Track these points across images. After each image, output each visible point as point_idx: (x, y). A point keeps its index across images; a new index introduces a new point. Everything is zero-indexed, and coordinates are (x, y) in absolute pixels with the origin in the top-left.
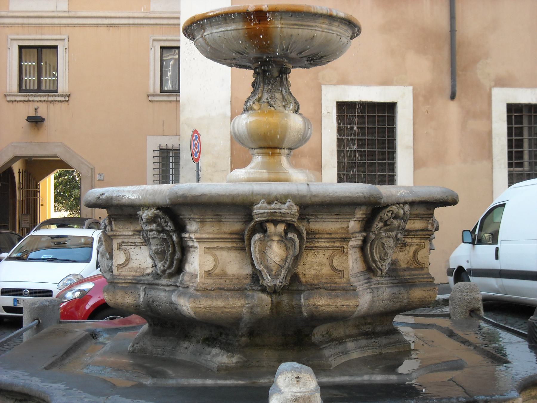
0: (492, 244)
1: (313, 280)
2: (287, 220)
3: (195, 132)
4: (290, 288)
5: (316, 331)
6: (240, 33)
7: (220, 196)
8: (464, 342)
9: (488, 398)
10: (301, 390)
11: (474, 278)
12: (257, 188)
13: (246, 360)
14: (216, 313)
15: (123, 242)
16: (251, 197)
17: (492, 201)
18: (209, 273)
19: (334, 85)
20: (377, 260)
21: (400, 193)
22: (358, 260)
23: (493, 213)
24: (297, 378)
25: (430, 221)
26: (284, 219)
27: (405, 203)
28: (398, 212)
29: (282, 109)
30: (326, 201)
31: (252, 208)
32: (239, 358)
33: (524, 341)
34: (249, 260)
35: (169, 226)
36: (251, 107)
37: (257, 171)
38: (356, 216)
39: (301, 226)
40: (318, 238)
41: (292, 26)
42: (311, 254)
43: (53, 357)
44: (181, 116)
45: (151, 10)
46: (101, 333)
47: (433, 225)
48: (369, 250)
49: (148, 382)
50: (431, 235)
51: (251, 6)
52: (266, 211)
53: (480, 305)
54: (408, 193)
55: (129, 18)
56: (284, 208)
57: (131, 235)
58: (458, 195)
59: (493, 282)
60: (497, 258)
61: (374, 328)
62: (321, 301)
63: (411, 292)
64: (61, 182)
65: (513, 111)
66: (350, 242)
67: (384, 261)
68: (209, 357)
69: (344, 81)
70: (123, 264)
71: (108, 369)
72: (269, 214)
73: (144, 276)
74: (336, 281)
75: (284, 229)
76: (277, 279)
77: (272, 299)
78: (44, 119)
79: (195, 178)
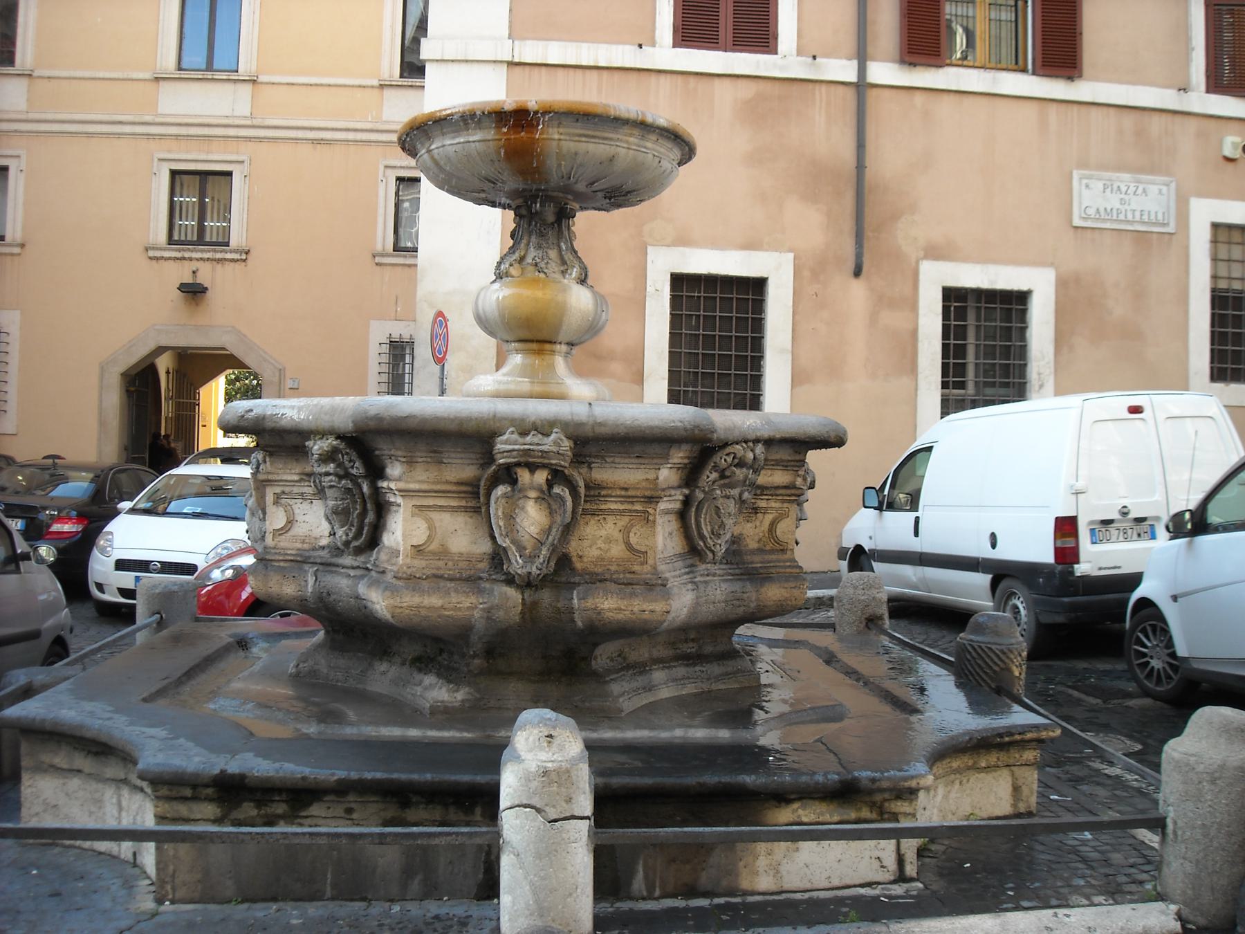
0: (910, 510)
1: (596, 565)
2: (552, 464)
3: (440, 314)
4: (556, 578)
5: (598, 651)
6: (489, 147)
7: (439, 419)
8: (851, 673)
9: (878, 775)
10: (555, 756)
11: (879, 564)
12: (505, 407)
13: (478, 696)
14: (428, 617)
15: (283, 493)
16: (492, 423)
17: (915, 440)
18: (418, 550)
19: (669, 246)
20: (707, 535)
21: (748, 423)
22: (674, 534)
23: (915, 461)
24: (548, 736)
25: (800, 473)
26: (546, 461)
27: (757, 441)
28: (744, 456)
29: (558, 276)
30: (619, 434)
31: (494, 441)
32: (469, 693)
33: (947, 673)
34: (486, 529)
35: (357, 468)
36: (507, 273)
37: (513, 379)
38: (670, 461)
39: (575, 474)
40: (604, 496)
41: (577, 138)
42: (593, 522)
43: (164, 679)
44: (418, 288)
45: (384, 119)
46: (255, 639)
47: (805, 479)
48: (693, 518)
49: (312, 729)
50: (799, 496)
51: (510, 102)
52: (516, 447)
53: (884, 611)
54: (763, 425)
55: (348, 130)
56: (548, 444)
57: (296, 481)
58: (845, 431)
59: (908, 571)
60: (916, 534)
61: (700, 647)
62: (606, 603)
63: (763, 590)
64: (239, 389)
65: (953, 300)
66: (659, 504)
67: (719, 538)
68: (419, 690)
69: (682, 240)
70: (282, 529)
71: (248, 703)
72: (521, 453)
73: (317, 550)
74: (633, 570)
75: (547, 480)
76: (533, 563)
77: (523, 596)
78: (206, 289)
79: (437, 391)
